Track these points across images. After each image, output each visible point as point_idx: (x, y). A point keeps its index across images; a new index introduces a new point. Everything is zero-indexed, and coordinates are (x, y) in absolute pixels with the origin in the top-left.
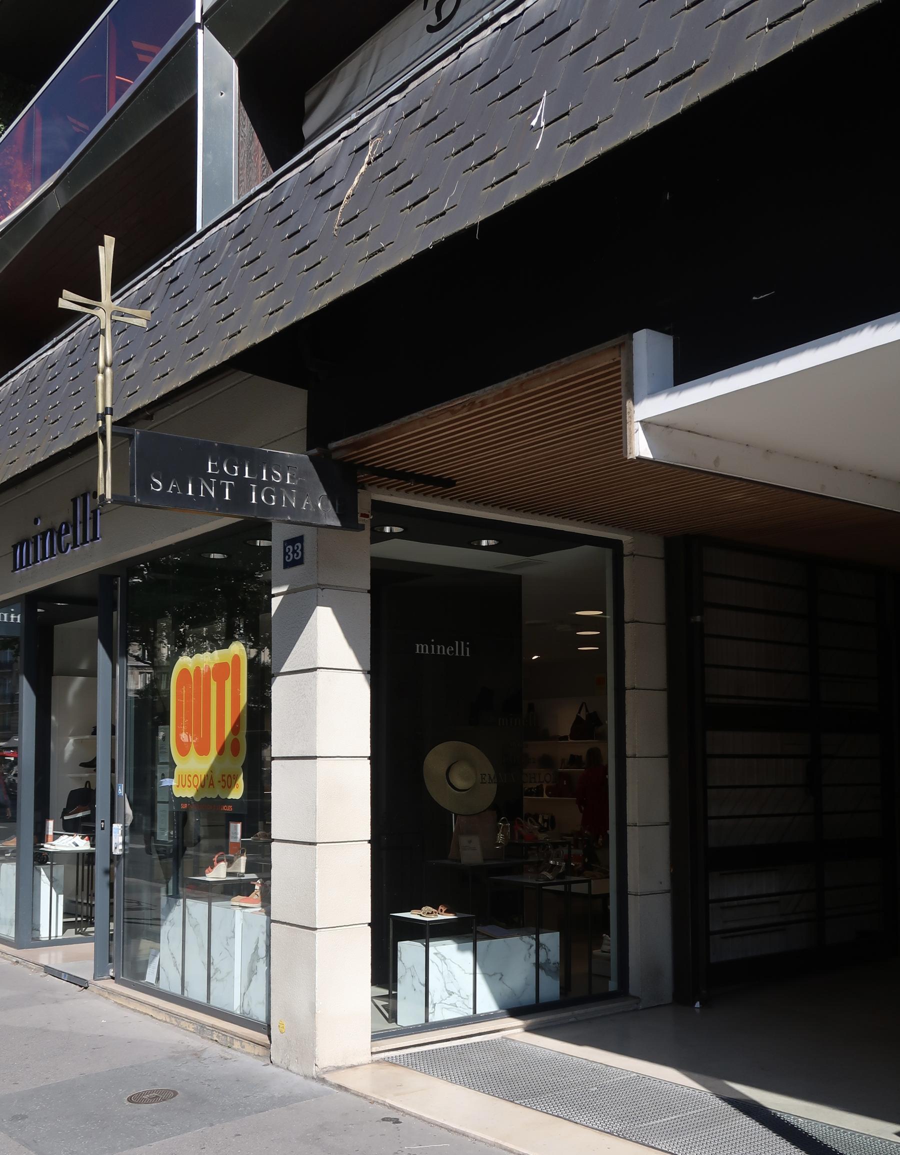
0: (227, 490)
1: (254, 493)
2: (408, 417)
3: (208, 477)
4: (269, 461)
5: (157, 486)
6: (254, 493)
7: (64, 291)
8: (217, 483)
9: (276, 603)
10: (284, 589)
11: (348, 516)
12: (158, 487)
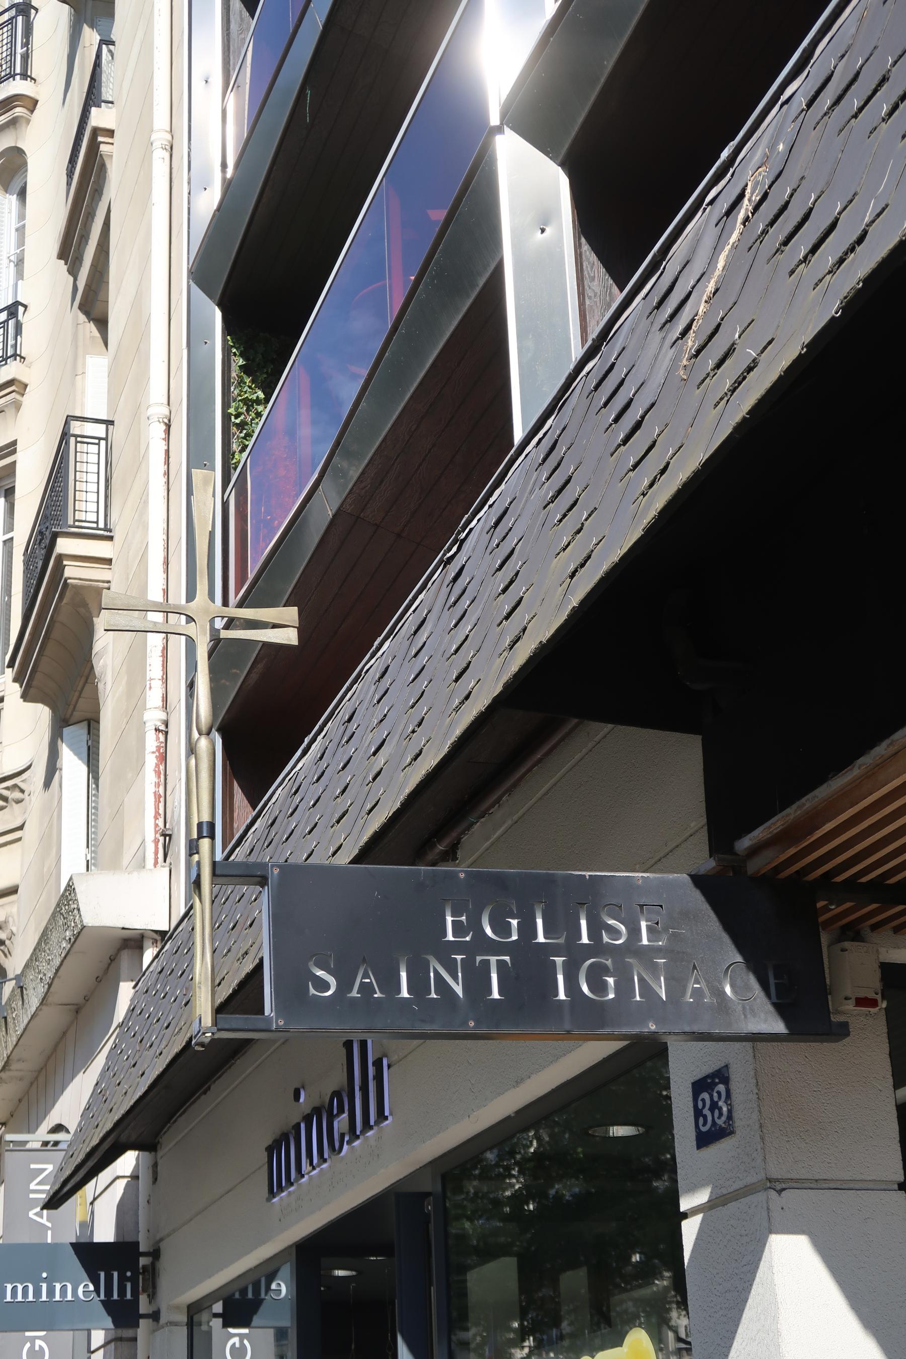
0: (494, 977)
1: (560, 978)
2: (884, 744)
3: (444, 953)
4: (591, 897)
5: (323, 985)
6: (560, 978)
7: (295, 642)
8: (468, 965)
9: (690, 1230)
10: (702, 1197)
11: (807, 1010)
12: (325, 986)
